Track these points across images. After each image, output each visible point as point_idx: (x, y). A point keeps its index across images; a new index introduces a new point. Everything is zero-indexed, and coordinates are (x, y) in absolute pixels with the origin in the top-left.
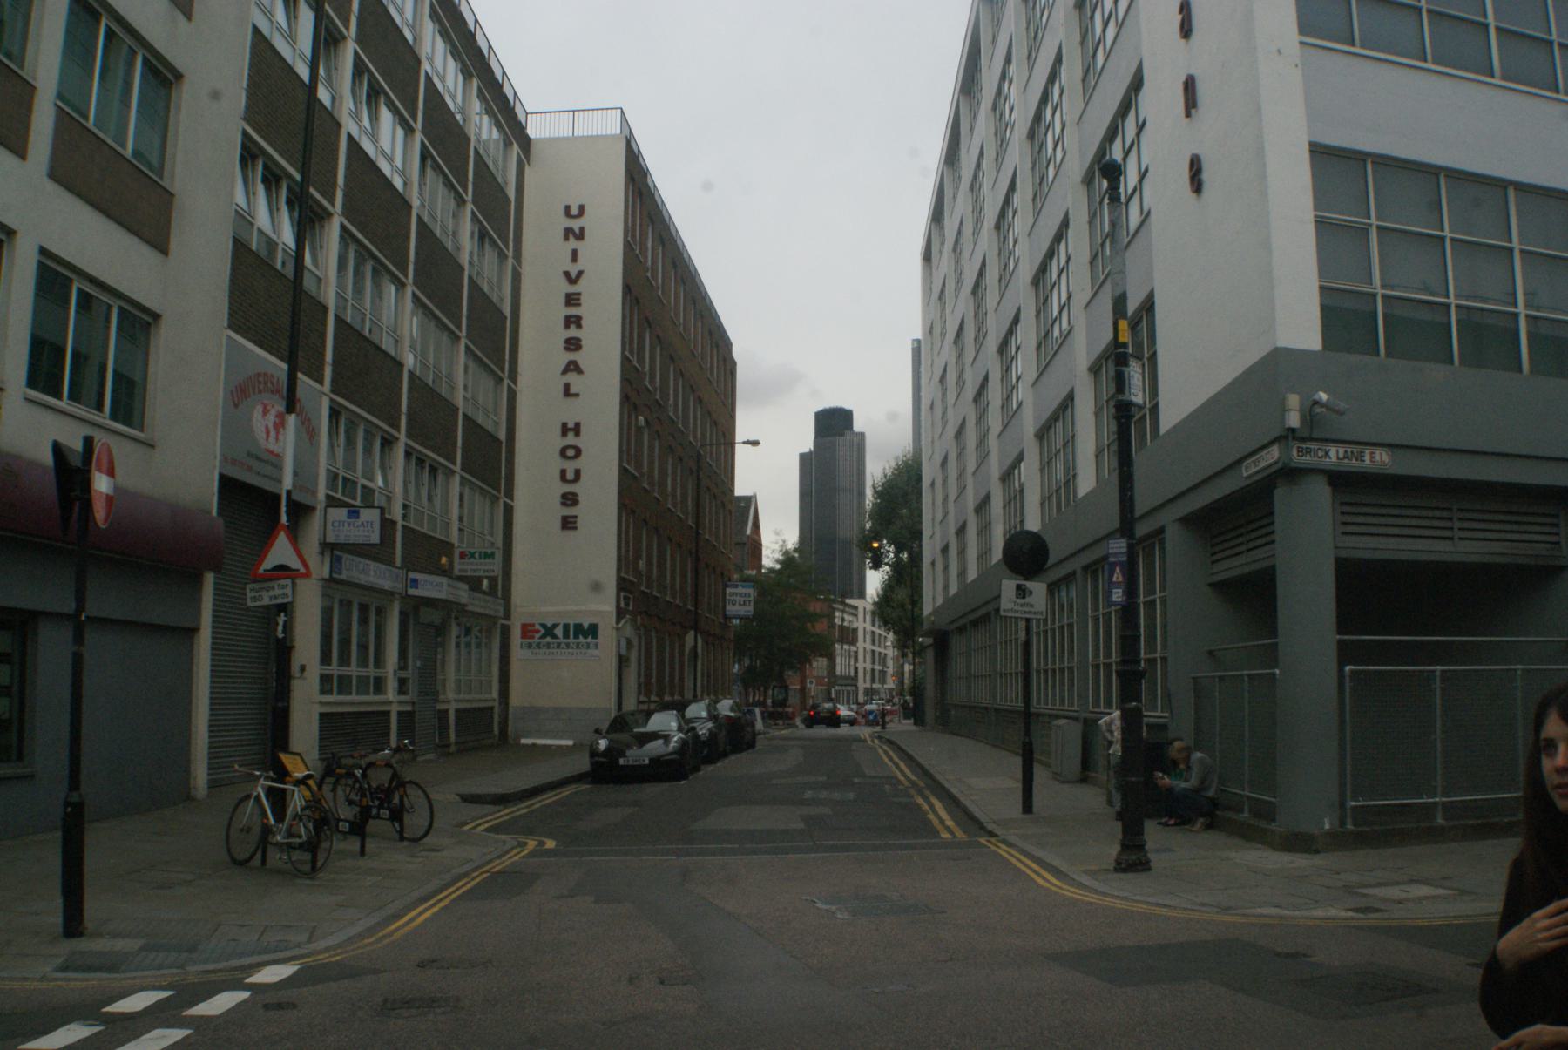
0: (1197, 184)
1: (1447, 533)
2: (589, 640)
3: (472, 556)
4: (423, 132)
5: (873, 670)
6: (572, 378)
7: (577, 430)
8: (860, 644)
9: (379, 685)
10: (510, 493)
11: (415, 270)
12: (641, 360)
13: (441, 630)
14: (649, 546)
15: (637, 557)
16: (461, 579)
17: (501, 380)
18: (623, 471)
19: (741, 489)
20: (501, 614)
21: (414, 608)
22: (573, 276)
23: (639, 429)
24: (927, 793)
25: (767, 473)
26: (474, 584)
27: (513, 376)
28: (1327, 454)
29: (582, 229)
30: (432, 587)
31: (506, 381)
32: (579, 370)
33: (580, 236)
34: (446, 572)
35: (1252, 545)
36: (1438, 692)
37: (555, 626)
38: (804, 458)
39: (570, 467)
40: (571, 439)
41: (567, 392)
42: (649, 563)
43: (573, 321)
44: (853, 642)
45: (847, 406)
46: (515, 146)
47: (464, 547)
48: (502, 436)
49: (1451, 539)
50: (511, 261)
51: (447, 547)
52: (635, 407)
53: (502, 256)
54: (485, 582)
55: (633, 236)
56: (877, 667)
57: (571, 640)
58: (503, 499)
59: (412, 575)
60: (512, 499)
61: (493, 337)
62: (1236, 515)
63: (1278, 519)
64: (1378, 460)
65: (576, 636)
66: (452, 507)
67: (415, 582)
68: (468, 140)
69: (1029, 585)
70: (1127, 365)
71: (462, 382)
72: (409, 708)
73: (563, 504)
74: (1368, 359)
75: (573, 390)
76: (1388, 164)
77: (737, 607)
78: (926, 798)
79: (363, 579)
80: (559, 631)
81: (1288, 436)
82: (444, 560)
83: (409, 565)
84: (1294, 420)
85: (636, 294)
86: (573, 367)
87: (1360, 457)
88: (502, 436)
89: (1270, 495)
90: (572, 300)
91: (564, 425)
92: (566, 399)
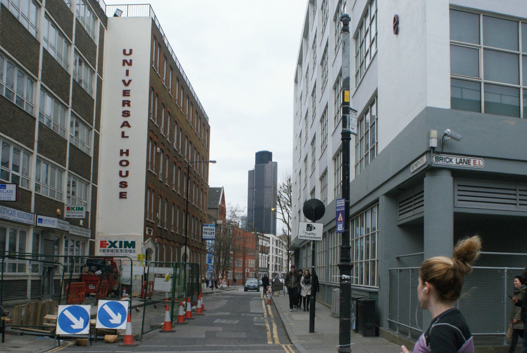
0: (396, 30)
1: (514, 202)
2: (131, 248)
3: (73, 209)
4: (46, 7)
5: (276, 266)
6: (125, 129)
7: (127, 153)
8: (271, 254)
9: (22, 268)
10: (95, 181)
11: (42, 74)
12: (159, 122)
13: (57, 243)
14: (163, 207)
15: (156, 211)
16: (67, 219)
17: (91, 129)
18: (148, 173)
19: (213, 182)
20: (90, 236)
21: (43, 233)
22: (127, 82)
23: (157, 153)
24: (273, 321)
25: (228, 176)
26: (74, 222)
27: (98, 127)
28: (451, 160)
29: (131, 61)
30: (50, 222)
31: (94, 130)
32: (129, 126)
33: (130, 64)
34: (60, 217)
35: (416, 206)
36: (506, 279)
37: (116, 242)
38: (250, 173)
39: (124, 170)
40: (124, 157)
41: (123, 135)
42: (163, 215)
43: (126, 103)
44: (267, 253)
45: (270, 151)
46: (99, 20)
47: (70, 205)
48: (92, 155)
49: (515, 204)
50: (96, 74)
51: (61, 205)
52: (155, 143)
53: (93, 72)
54: (81, 221)
55: (156, 65)
56: (278, 264)
57: (123, 248)
58: (91, 184)
59: (39, 217)
60: (96, 184)
61: (86, 109)
62: (407, 192)
63: (425, 194)
64: (478, 164)
65: (125, 247)
66: (61, 185)
67: (41, 220)
68: (73, 15)
69: (314, 224)
70: (348, 113)
71: (67, 127)
72: (38, 279)
73: (121, 187)
74: (478, 114)
75: (125, 135)
76: (490, 16)
77: (208, 235)
78: (271, 324)
79: (11, 218)
80: (117, 245)
81: (432, 150)
82: (58, 210)
83: (38, 212)
84: (434, 143)
85: (155, 90)
86: (126, 124)
87: (468, 162)
88: (92, 155)
89: (422, 182)
90: (126, 93)
91: (121, 151)
92: (122, 140)
